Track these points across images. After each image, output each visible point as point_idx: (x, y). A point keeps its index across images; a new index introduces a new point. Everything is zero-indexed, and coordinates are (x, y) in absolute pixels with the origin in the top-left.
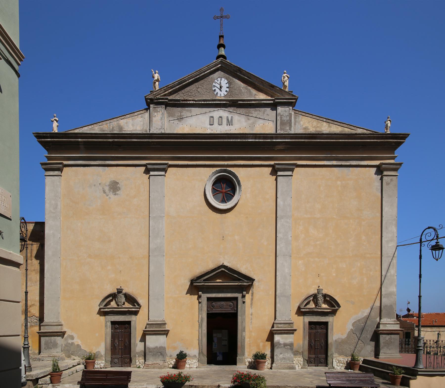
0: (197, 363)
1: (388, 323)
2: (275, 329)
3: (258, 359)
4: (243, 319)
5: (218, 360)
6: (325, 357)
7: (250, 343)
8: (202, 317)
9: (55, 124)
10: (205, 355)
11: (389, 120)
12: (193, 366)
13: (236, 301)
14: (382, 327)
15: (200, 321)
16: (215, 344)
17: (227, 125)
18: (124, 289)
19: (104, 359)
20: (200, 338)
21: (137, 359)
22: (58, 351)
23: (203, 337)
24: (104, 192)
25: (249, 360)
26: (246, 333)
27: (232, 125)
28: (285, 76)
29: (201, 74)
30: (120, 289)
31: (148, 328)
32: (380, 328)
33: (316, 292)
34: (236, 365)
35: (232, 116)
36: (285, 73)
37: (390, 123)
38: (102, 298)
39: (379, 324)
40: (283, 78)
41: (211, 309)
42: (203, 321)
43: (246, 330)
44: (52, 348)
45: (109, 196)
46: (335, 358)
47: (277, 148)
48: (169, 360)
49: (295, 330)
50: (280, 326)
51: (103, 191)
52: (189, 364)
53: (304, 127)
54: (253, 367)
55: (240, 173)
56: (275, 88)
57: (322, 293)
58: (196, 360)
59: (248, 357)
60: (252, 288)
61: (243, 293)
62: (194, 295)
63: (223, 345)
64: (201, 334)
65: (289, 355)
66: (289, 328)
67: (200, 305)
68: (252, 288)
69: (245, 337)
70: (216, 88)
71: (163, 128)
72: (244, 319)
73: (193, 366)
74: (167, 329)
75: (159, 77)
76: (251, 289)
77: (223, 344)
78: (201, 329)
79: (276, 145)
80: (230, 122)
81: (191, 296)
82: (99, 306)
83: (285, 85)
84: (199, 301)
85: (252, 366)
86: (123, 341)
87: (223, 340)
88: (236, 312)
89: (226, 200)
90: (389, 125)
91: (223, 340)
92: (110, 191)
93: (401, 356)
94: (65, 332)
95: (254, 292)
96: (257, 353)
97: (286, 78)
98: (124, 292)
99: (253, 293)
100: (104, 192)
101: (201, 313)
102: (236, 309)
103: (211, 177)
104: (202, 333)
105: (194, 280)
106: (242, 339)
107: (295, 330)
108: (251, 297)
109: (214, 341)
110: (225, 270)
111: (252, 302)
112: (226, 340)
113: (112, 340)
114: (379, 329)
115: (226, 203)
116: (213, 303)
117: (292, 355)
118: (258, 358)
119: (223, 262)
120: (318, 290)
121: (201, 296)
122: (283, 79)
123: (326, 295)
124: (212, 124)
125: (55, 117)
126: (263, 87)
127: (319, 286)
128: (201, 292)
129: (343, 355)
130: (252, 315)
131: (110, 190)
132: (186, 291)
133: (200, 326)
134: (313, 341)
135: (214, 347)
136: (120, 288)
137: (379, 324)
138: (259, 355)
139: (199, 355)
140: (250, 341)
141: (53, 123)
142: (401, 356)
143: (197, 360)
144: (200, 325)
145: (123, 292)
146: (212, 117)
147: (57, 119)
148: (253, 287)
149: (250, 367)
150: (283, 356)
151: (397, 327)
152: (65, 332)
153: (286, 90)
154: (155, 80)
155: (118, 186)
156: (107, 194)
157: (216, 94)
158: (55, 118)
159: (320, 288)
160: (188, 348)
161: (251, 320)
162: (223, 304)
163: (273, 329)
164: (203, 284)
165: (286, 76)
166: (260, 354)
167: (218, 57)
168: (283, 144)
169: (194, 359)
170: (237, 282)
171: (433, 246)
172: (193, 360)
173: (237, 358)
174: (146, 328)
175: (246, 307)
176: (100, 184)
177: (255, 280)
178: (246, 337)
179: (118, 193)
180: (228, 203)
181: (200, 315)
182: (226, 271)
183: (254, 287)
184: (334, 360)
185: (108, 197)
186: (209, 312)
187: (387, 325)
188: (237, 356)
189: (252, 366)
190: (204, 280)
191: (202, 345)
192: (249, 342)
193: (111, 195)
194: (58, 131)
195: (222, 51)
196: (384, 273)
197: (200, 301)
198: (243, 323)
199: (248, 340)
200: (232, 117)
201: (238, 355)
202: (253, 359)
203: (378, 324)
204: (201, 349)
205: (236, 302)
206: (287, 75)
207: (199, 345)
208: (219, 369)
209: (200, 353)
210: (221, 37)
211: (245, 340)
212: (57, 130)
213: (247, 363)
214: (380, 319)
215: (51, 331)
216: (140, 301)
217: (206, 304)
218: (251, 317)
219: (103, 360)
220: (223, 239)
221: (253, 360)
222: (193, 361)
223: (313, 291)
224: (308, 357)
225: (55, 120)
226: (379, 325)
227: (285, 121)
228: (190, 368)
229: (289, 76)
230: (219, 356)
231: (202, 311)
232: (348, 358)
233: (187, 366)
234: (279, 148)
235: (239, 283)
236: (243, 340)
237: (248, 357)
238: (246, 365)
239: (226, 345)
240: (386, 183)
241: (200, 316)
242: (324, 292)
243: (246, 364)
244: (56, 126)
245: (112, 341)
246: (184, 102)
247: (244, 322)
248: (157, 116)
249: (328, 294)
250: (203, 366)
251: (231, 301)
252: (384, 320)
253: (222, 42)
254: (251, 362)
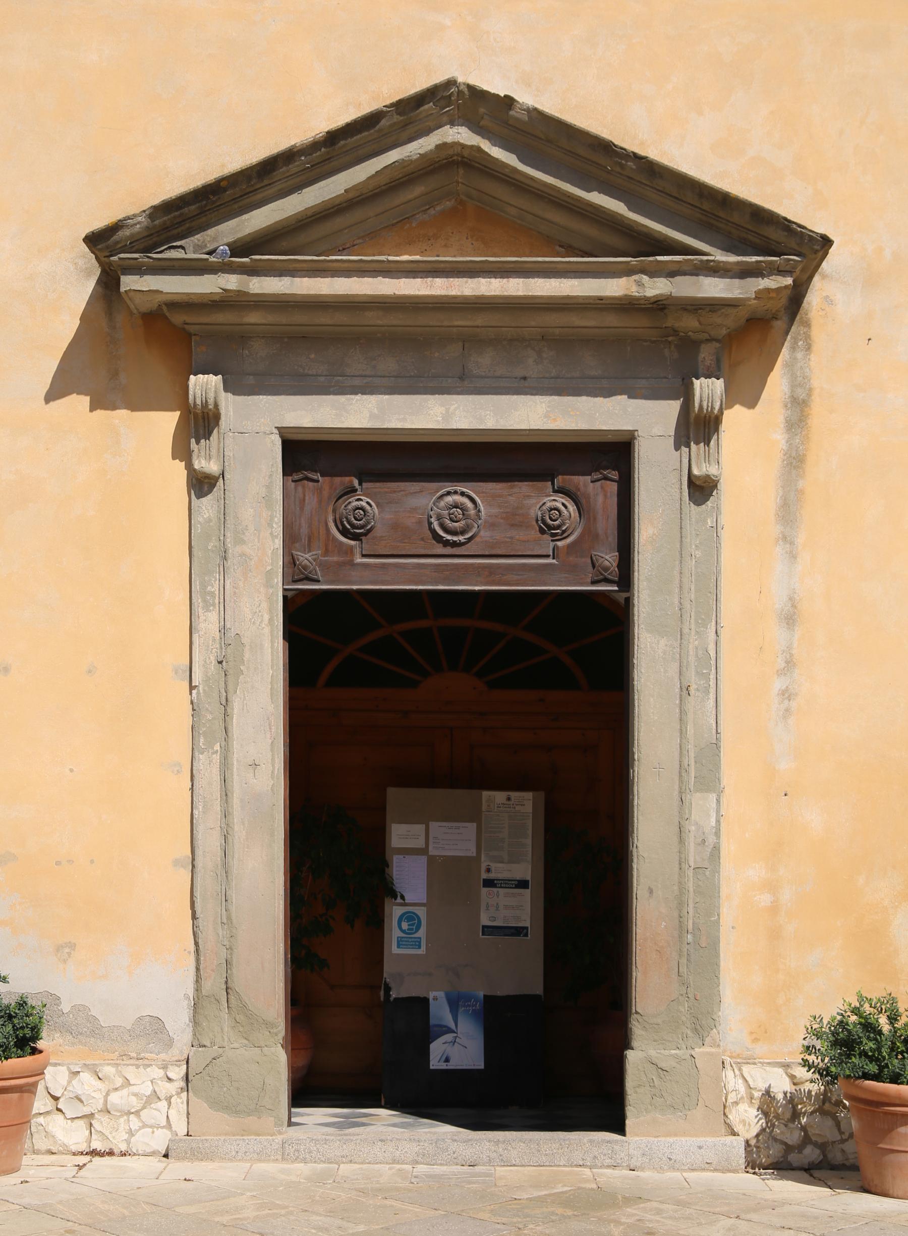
0: (179, 1102)
3: (877, 1078)
4: (692, 658)
5: (435, 1063)
7: (774, 909)
8: (223, 630)
10: (268, 1025)
12: (131, 1133)
13: (614, 475)
16: (410, 917)
20: (210, 842)
23: (239, 830)
25: (763, 1086)
26: (724, 800)
29: (638, 798)
34: (619, 1128)
41: (326, 552)
43: (729, 775)
52: (86, 1110)
54: (811, 1154)
58: (165, 1067)
59: (760, 1049)
60: (793, 348)
61: (687, 394)
62: (134, 407)
63: (487, 930)
64: (217, 807)
67: (207, 506)
68: (793, 348)
69: (716, 849)
73: (131, 1133)
76: (785, 353)
77: (485, 921)
78: (216, 758)
81: (100, 413)
84: (189, 467)
85: (807, 1140)
87: (489, 883)
91: (489, 883)
95: (815, 383)
96: (856, 1011)
99: (801, 394)
101: (215, 588)
102: (609, 559)
104: (226, 795)
105: (126, 232)
106: (682, 862)
108: (779, 437)
109: (393, 894)
110: (486, 146)
111: (801, 492)
112: (522, 884)
114: (543, 997)
116: (352, 491)
118: (873, 1068)
121: (217, 417)
128: (214, 380)
130: (790, 619)
132: (52, 365)
135: (393, 948)
138: (886, 1028)
139: (195, 1022)
140: (772, 886)
143: (177, 1073)
144: (211, 713)
148: (808, 338)
149: (775, 1151)
160: (72, 946)
161: (781, 673)
162: (464, 509)
164: (231, 282)
166: (892, 1019)
169: (140, 1061)
170: (628, 272)
172: (130, 1073)
175: (724, 534)
178: (729, 849)
181: (207, 607)
182: (496, 152)
183: (818, 334)
188: (624, 1042)
189: (800, 1148)
190: (241, 248)
191: (228, 922)
192: (765, 899)
197: (206, 464)
198: (691, 703)
199: (756, 872)
201: (638, 1030)
202: (809, 1075)
204: (211, 961)
205: (613, 487)
207: (194, 917)
208: (422, 1168)
211: (716, 870)
213: (743, 1107)
217: (268, 500)
218: (790, 647)
221: (808, 1086)
222: (127, 1083)
228: (94, 1153)
230: (450, 1031)
233: (61, 1136)
235: (639, 284)
237: (760, 1049)
238: (734, 1134)
239: (519, 931)
241: (209, 623)
243: (733, 1117)
247: (707, 691)
250: (246, 1132)
251: (559, 480)
254: (792, 1101)
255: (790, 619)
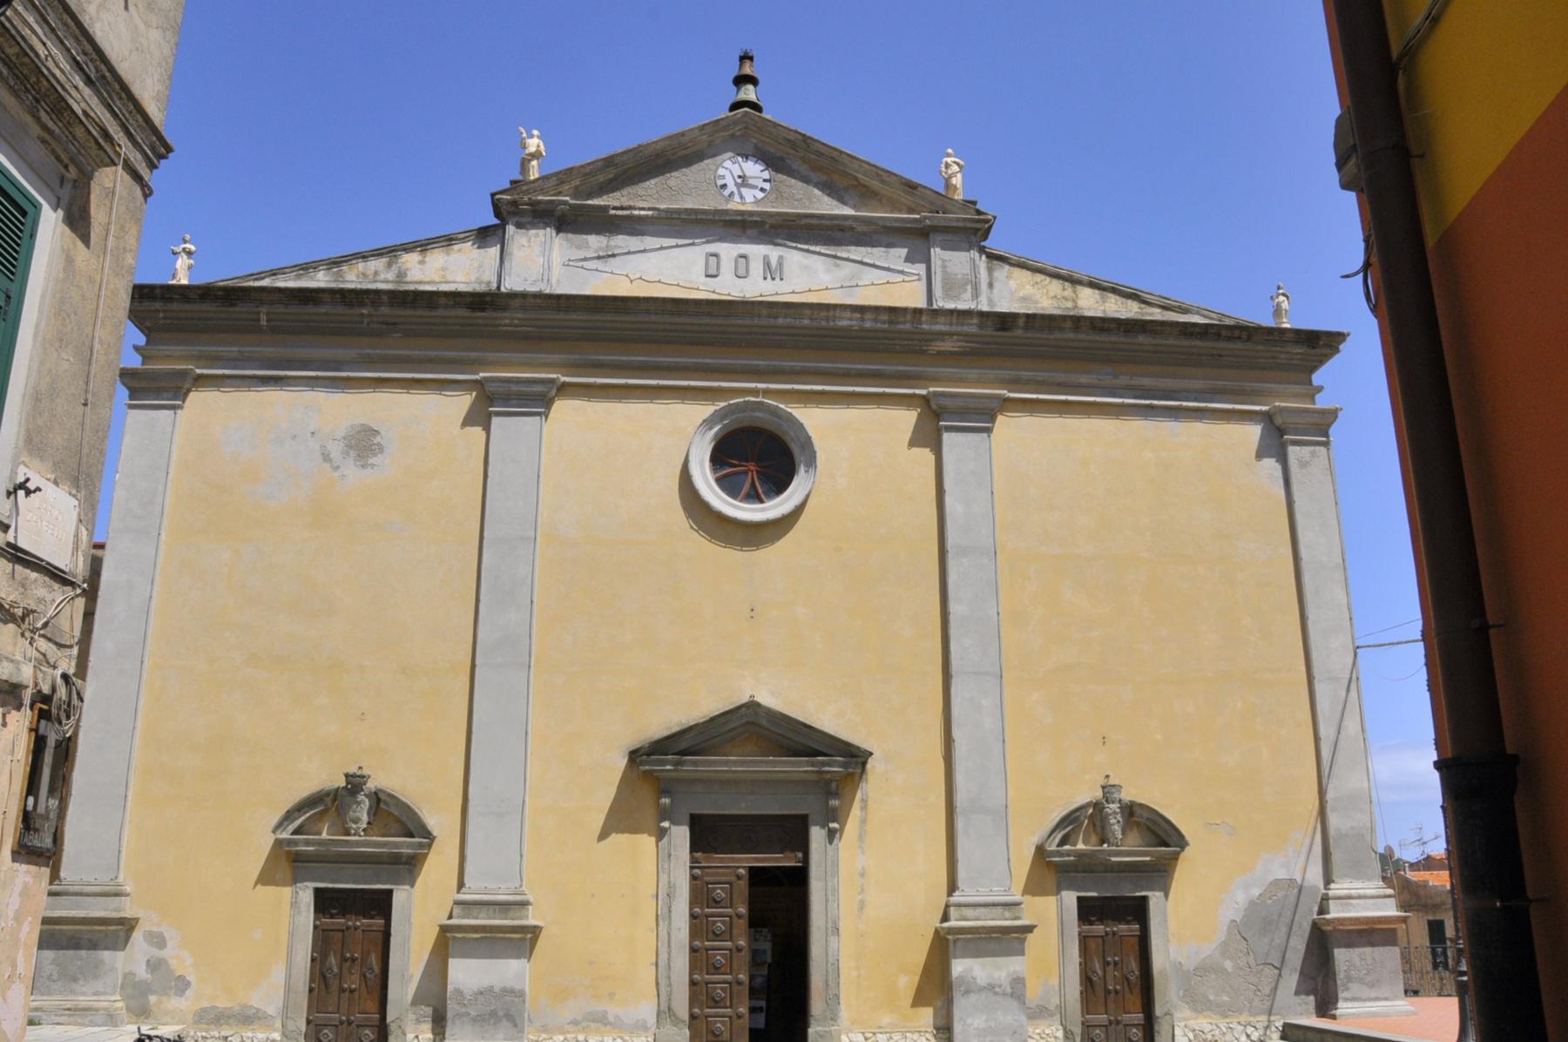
1: (1356, 895)
2: (952, 923)
6: (1142, 1022)
8: (669, 882)
9: (182, 263)
10: (683, 1022)
11: (1283, 294)
14: (1336, 912)
15: (662, 895)
17: (765, 278)
18: (372, 777)
19: (278, 1024)
21: (408, 1029)
22: (101, 990)
23: (674, 952)
24: (326, 457)
27: (782, 279)
28: (949, 162)
30: (359, 776)
31: (459, 917)
32: (1328, 913)
33: (1099, 794)
35: (781, 254)
36: (948, 155)
37: (1286, 302)
38: (288, 806)
39: (1325, 898)
40: (943, 166)
42: (674, 896)
44: (80, 976)
45: (342, 469)
46: (1182, 1024)
47: (936, 348)
48: (540, 1036)
49: (1029, 929)
50: (969, 912)
51: (323, 454)
53: (1021, 295)
55: (815, 420)
56: (919, 189)
57: (1120, 801)
65: (1010, 1015)
66: (1006, 919)
70: (726, 173)
71: (545, 278)
72: (836, 891)
74: (531, 921)
75: (542, 148)
79: (932, 340)
80: (776, 269)
82: (274, 832)
83: (953, 185)
86: (359, 960)
88: (800, 864)
89: (764, 492)
90: (1285, 305)
92: (348, 455)
93: (1412, 1008)
94: (137, 920)
97: (956, 168)
98: (371, 785)
99: (865, 797)
100: (326, 457)
103: (708, 423)
106: (827, 961)
107: (1029, 929)
113: (315, 955)
114: (1327, 916)
115: (761, 501)
117: (1023, 1018)
119: (751, 693)
120: (1106, 790)
122: (943, 169)
123: (1135, 809)
124: (714, 272)
125: (185, 242)
126: (881, 185)
127: (1107, 776)
129: (1209, 1013)
130: (862, 875)
131: (346, 454)
133: (662, 917)
134: (1098, 967)
136: (359, 773)
137: (1325, 898)
141: (177, 259)
142: (1412, 1008)
145: (368, 785)
146: (716, 255)
147: (193, 248)
150: (986, 1021)
151: (1390, 910)
152: (137, 920)
153: (956, 197)
154: (527, 155)
155: (378, 439)
156: (336, 465)
157: (730, 196)
158: (188, 246)
159: (1111, 782)
161: (860, 894)
163: (946, 925)
165: (955, 162)
167: (736, 106)
168: (955, 337)
171: (1422, 635)
173: (811, 1031)
174: (450, 917)
176: (313, 433)
177: (871, 754)
179: (375, 463)
180: (768, 504)
184: (1178, 1032)
185: (336, 474)
186: (700, 863)
187: (1352, 901)
193: (351, 470)
194: (189, 280)
195: (749, 93)
196: (1327, 732)
200: (781, 258)
201: (812, 1021)
203: (1322, 899)
206: (957, 160)
209: (665, 1013)
210: (746, 57)
212: (187, 278)
214: (1328, 880)
215: (82, 915)
216: (431, 821)
219: (275, 1030)
220: (752, 617)
223: (1087, 794)
224: (1083, 1024)
225: (184, 249)
226: (1325, 902)
227: (959, 276)
229: (962, 163)
231: (670, 862)
232: (1228, 1020)
234: (942, 349)
236: (829, 965)
240: (1296, 461)
241: (664, 879)
242: (1127, 795)
244: (186, 268)
245: (313, 960)
246: (620, 213)
248: (529, 246)
249: (1143, 802)
252: (1339, 888)
253: (747, 70)
255: (862, 875)
